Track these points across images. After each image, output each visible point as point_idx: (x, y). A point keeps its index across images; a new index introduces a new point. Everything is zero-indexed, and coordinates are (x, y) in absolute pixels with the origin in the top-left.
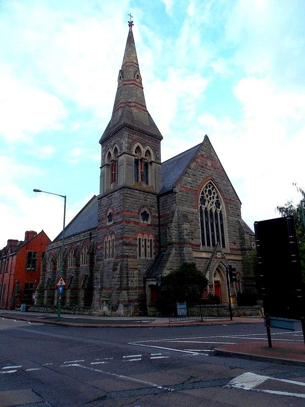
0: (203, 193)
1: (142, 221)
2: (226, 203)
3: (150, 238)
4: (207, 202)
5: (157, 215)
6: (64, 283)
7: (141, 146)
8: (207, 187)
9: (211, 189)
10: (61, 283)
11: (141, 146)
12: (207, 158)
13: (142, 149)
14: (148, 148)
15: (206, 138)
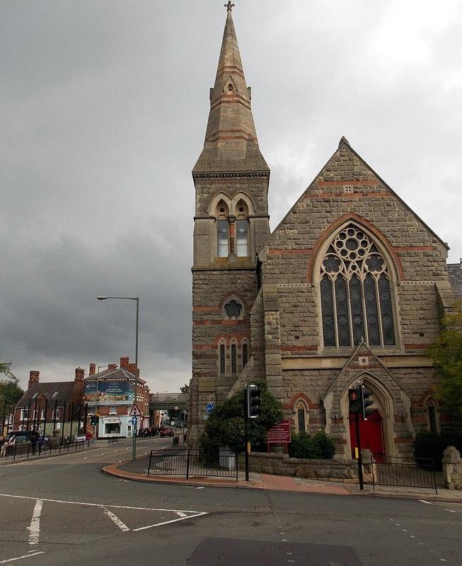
0: (331, 249)
1: (227, 318)
7: (225, 199)
8: (342, 236)
11: (225, 199)
12: (343, 180)
13: (229, 202)
14: (239, 196)
15: (343, 142)
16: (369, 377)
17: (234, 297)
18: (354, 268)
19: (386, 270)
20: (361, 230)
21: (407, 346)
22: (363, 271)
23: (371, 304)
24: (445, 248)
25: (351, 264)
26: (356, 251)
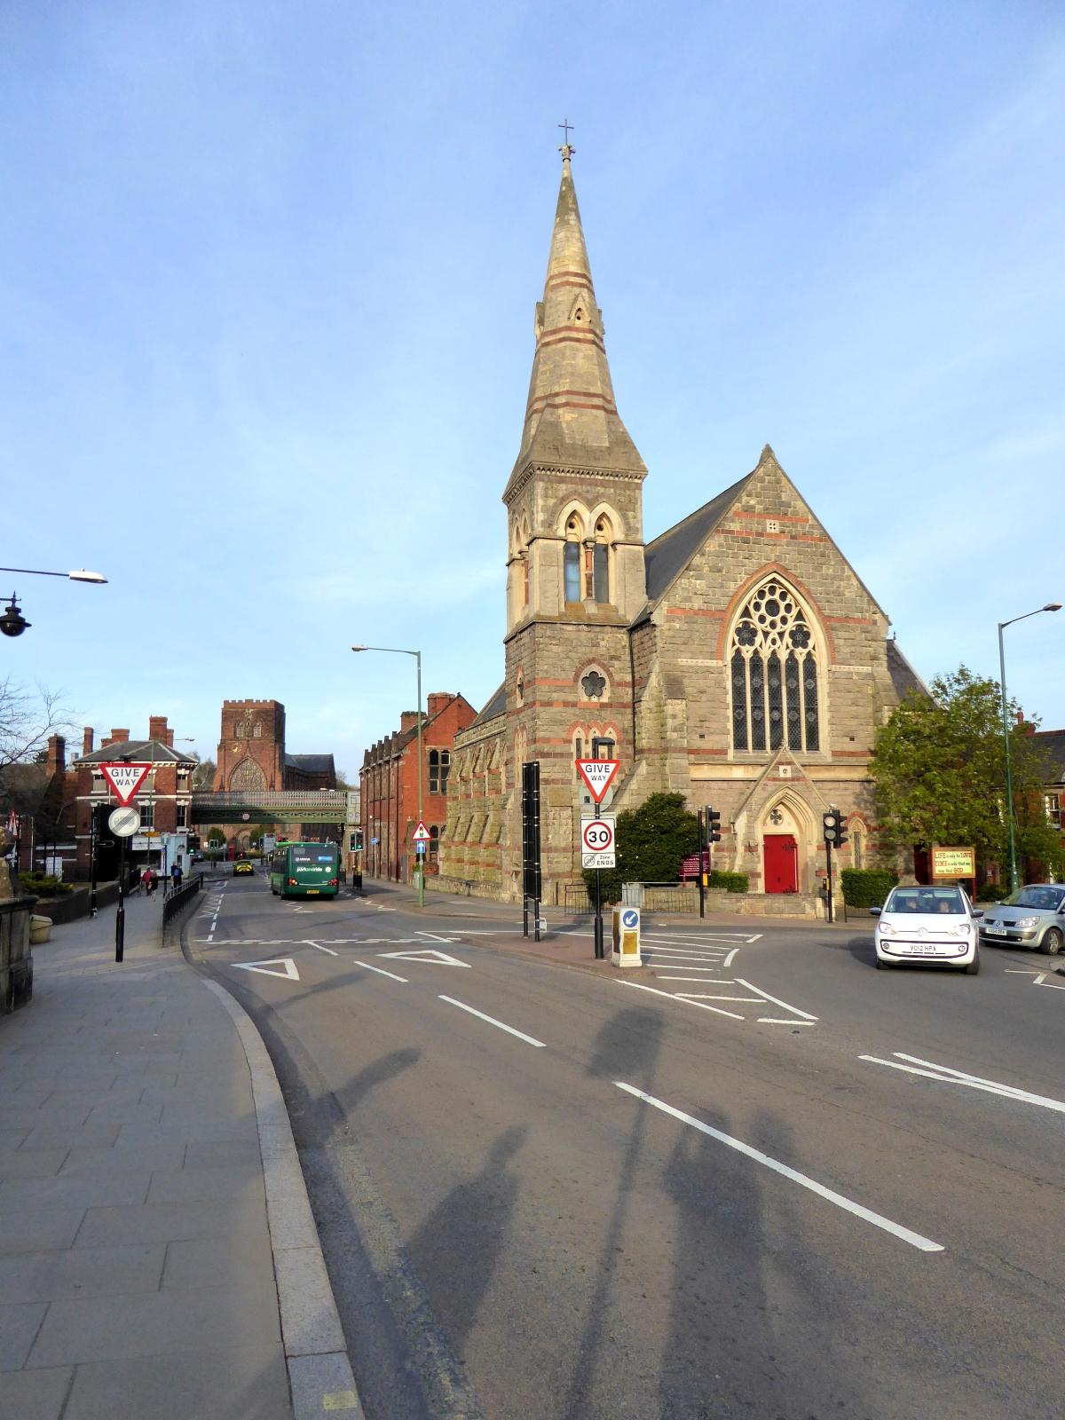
0: (746, 613)
1: (585, 699)
2: (829, 631)
5: (629, 678)
8: (761, 594)
9: (776, 597)
10: (421, 835)
12: (767, 513)
16: (791, 793)
17: (595, 668)
18: (774, 642)
19: (814, 648)
20: (785, 588)
21: (835, 754)
22: (785, 647)
23: (793, 694)
24: (885, 622)
25: (770, 637)
26: (777, 619)
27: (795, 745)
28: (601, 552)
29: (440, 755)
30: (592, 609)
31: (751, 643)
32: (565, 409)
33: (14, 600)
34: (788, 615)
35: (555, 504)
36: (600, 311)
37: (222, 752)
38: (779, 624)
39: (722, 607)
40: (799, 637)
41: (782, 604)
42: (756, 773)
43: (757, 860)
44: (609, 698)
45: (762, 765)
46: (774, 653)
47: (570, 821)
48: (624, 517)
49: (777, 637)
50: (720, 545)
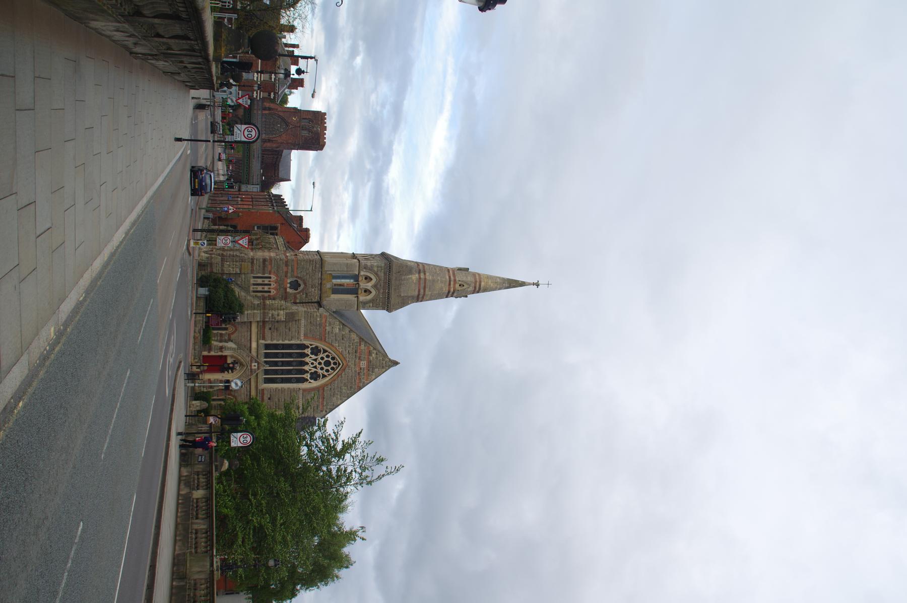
0: (325, 351)
1: (289, 281)
3: (272, 291)
4: (315, 357)
6: (230, 211)
8: (333, 358)
9: (332, 365)
10: (230, 209)
12: (369, 362)
16: (245, 368)
17: (302, 286)
18: (312, 364)
19: (310, 382)
21: (263, 390)
23: (289, 372)
25: (314, 362)
27: (267, 372)
28: (354, 291)
29: (275, 231)
30: (329, 286)
31: (312, 353)
32: (418, 277)
33: (307, 72)
34: (324, 371)
35: (374, 271)
36: (466, 296)
37: (292, 111)
38: (320, 366)
39: (327, 340)
40: (315, 376)
41: (329, 368)
42: (254, 353)
43: (216, 351)
44: (289, 293)
45: (257, 356)
46: (308, 364)
47: (235, 272)
48: (370, 301)
49: (315, 365)
50: (354, 340)
